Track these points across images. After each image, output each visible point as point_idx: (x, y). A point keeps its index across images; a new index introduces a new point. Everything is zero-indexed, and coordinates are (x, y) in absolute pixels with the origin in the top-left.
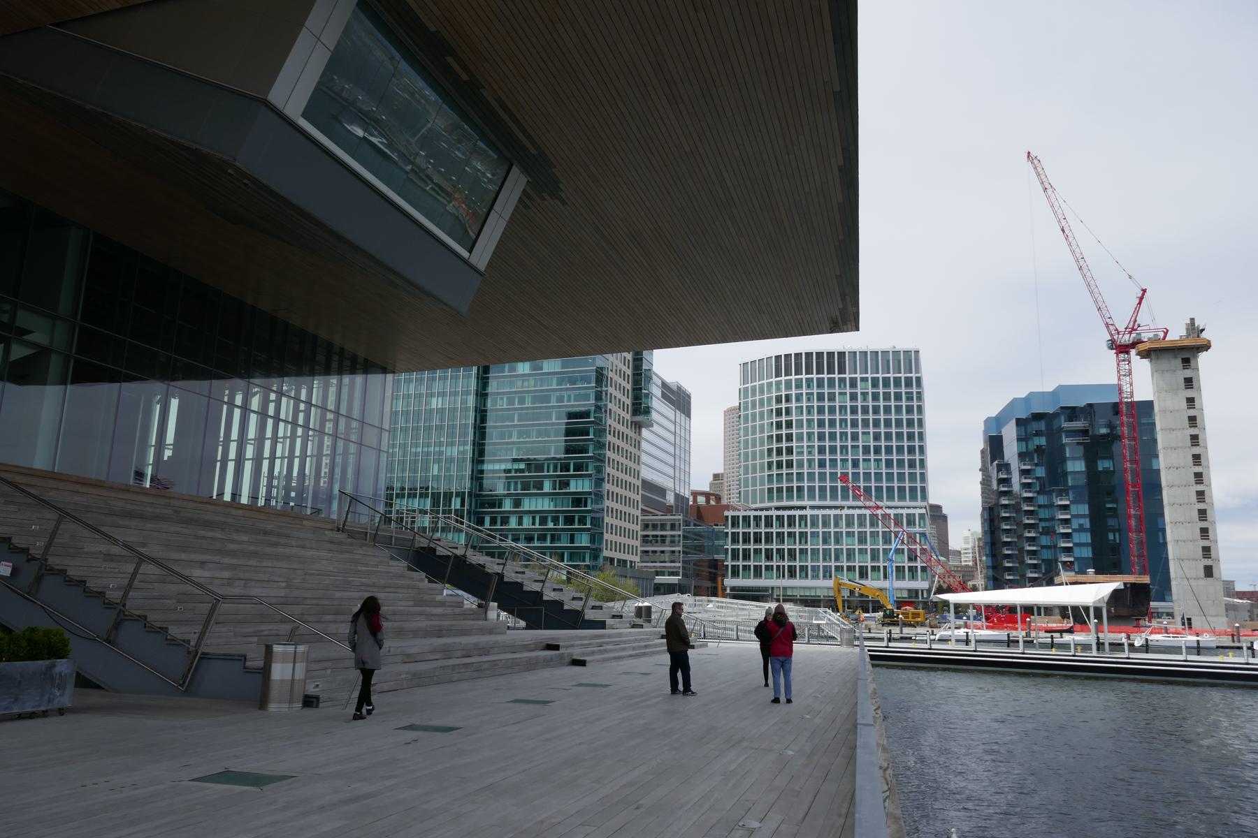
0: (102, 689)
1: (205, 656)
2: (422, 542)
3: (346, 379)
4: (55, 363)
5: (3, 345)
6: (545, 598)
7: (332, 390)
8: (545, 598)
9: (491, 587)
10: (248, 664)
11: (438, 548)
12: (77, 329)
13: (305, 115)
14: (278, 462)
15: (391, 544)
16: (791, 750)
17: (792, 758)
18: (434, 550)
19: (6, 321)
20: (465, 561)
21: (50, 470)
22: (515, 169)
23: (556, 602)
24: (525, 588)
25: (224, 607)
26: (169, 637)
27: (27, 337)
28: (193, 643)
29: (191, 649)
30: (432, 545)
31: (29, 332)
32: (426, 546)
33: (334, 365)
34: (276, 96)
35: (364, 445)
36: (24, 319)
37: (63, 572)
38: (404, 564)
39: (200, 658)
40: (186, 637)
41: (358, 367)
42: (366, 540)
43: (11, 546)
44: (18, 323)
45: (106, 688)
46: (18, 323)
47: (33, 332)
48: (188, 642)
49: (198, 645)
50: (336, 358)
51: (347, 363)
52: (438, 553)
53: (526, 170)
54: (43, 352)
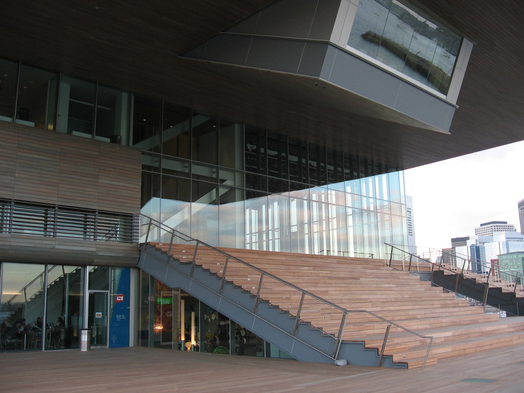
0: (298, 361)
1: (343, 343)
2: (436, 269)
3: (377, 177)
4: (238, 193)
5: (215, 189)
6: (517, 296)
7: (370, 184)
8: (517, 296)
9: (485, 293)
10: (366, 346)
11: (445, 271)
12: (245, 175)
13: (349, 44)
14: (335, 227)
15: (417, 271)
16: (249, 278)
17: (288, 313)
18: (443, 272)
19: (215, 177)
20: (463, 277)
21: (244, 248)
22: (465, 41)
23: (498, 288)
24: (503, 291)
25: (349, 316)
26: (323, 333)
27: (225, 183)
28: (336, 335)
29: (336, 339)
30: (441, 269)
31: (225, 180)
32: (438, 270)
33: (369, 171)
34: (333, 39)
35: (347, 192)
36: (223, 174)
37: (267, 302)
38: (430, 282)
39: (341, 343)
40: (332, 332)
41: (383, 170)
42: (403, 270)
43: (242, 290)
44: (220, 177)
45: (299, 360)
46: (220, 177)
47: (227, 180)
48: (334, 335)
49: (339, 336)
50: (369, 167)
51: (376, 169)
52: (445, 274)
53: (471, 39)
54: (232, 189)
